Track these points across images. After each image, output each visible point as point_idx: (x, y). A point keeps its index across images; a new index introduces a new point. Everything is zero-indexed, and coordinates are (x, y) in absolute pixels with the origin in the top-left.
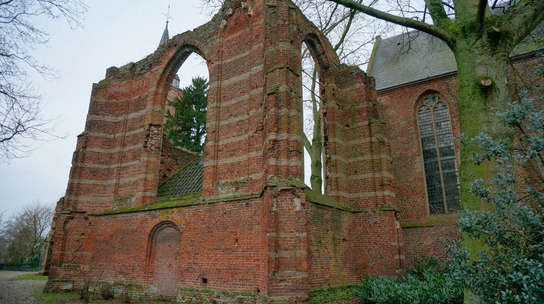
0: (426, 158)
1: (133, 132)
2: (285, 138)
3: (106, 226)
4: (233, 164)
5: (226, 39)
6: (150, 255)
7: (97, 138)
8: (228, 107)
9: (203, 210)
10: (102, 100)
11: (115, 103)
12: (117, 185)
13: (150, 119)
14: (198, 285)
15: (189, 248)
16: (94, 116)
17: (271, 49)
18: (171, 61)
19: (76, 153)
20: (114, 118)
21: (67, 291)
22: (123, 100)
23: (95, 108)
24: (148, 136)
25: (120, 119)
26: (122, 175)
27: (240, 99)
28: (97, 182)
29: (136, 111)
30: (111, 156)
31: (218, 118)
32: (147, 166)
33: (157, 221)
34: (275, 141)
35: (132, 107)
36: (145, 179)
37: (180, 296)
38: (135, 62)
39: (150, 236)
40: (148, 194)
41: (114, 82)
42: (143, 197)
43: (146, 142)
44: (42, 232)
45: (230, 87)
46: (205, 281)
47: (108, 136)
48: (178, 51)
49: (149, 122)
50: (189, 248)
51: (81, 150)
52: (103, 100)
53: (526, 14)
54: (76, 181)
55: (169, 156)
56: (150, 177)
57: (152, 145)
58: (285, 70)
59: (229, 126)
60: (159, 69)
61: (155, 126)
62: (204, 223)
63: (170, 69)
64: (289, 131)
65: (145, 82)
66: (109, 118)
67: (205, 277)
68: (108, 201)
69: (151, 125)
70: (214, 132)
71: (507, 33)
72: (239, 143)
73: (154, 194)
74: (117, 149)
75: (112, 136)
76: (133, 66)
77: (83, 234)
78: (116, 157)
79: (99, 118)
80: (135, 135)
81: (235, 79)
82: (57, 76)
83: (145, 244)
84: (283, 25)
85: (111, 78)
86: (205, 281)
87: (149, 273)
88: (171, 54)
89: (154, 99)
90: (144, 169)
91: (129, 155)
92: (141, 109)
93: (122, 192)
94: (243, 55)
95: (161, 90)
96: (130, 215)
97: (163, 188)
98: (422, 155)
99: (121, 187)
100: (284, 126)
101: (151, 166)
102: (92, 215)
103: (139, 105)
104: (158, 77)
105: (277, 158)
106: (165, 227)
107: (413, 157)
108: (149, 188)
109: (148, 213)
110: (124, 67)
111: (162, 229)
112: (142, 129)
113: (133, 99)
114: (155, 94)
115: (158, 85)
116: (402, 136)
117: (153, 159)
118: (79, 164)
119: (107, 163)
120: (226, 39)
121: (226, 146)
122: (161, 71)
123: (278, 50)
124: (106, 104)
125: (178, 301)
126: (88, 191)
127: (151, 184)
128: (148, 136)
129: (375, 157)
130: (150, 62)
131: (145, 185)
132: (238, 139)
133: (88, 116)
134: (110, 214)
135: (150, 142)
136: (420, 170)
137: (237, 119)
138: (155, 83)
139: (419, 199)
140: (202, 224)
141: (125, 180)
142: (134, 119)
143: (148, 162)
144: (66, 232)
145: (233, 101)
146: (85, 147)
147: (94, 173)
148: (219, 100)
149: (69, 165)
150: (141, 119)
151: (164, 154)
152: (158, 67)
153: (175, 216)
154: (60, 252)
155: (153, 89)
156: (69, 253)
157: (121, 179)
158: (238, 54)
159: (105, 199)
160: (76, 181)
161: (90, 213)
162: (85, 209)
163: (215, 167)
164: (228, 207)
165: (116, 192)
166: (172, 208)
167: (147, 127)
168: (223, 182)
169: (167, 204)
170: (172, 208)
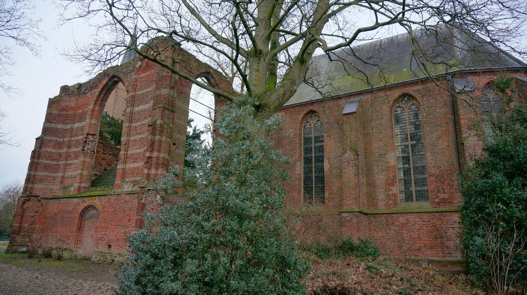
0: (305, 163)
1: (76, 138)
2: (156, 156)
3: (53, 207)
4: (134, 168)
5: (140, 76)
6: (80, 228)
7: (50, 141)
8: (135, 127)
10: (55, 112)
11: (66, 114)
12: (63, 177)
13: (87, 130)
14: (105, 250)
15: (103, 224)
17: (158, 92)
18: (104, 86)
19: (34, 152)
20: (64, 126)
21: (24, 252)
22: (71, 112)
23: (49, 118)
24: (85, 142)
25: (68, 127)
26: (67, 170)
27: (143, 122)
28: (49, 174)
29: (80, 122)
32: (83, 165)
33: (86, 205)
34: (149, 157)
35: (77, 118)
36: (81, 174)
37: (94, 257)
38: (82, 83)
39: (80, 215)
40: (83, 185)
41: (65, 98)
42: (79, 187)
43: (84, 147)
45: (138, 113)
46: (110, 246)
47: (59, 140)
48: (109, 80)
49: (87, 132)
50: (103, 224)
51: (38, 150)
52: (56, 112)
53: (279, 93)
54: (33, 173)
55: (110, 154)
56: (85, 172)
57: (88, 149)
58: (161, 109)
59: (135, 141)
60: (97, 91)
61: (91, 135)
62: (113, 208)
63: (104, 92)
64: (159, 151)
65: (87, 100)
66: (60, 126)
67: (110, 244)
68: (56, 189)
69: (88, 134)
70: (125, 144)
72: (140, 153)
74: (65, 150)
75: (62, 140)
76: (80, 85)
77: (36, 212)
78: (63, 156)
79: (52, 125)
80: (77, 141)
81: (142, 107)
82: (20, 93)
83: (77, 221)
84: (166, 76)
85: (63, 95)
86: (110, 246)
87: (79, 241)
88: (104, 82)
89: (92, 115)
90: (81, 167)
91: (73, 155)
92: (83, 121)
93: (66, 182)
94: (148, 90)
95: (97, 108)
96: (69, 199)
100: (156, 148)
101: (86, 165)
103: (82, 118)
104: (95, 99)
105: (150, 169)
106: (91, 210)
107: (295, 162)
108: (84, 180)
109: (80, 199)
110: (73, 86)
111: (89, 211)
112: (81, 137)
113: (78, 112)
114: (93, 111)
115: (95, 104)
116: (289, 145)
117: (88, 160)
118: (36, 161)
119: (57, 160)
120: (140, 76)
121: (132, 155)
122: (97, 93)
123: (161, 94)
125: (93, 259)
126: (41, 181)
127: (85, 178)
128: (85, 142)
130: (91, 85)
133: (44, 123)
134: (56, 198)
135: (87, 147)
136: (298, 172)
137: (140, 136)
138: (93, 103)
139: (296, 194)
140: (112, 208)
141: (68, 174)
142: (78, 128)
144: (24, 210)
145: (139, 123)
147: (47, 167)
148: (131, 122)
150: (82, 128)
151: (105, 152)
152: (95, 90)
153: (96, 202)
154: (18, 225)
155: (91, 107)
157: (66, 173)
158: (145, 88)
159: (54, 187)
160: (33, 173)
161: (42, 197)
162: (38, 194)
164: (128, 198)
165: (62, 182)
166: (95, 196)
167: (85, 136)
168: (127, 180)
169: (93, 193)
170: (95, 196)
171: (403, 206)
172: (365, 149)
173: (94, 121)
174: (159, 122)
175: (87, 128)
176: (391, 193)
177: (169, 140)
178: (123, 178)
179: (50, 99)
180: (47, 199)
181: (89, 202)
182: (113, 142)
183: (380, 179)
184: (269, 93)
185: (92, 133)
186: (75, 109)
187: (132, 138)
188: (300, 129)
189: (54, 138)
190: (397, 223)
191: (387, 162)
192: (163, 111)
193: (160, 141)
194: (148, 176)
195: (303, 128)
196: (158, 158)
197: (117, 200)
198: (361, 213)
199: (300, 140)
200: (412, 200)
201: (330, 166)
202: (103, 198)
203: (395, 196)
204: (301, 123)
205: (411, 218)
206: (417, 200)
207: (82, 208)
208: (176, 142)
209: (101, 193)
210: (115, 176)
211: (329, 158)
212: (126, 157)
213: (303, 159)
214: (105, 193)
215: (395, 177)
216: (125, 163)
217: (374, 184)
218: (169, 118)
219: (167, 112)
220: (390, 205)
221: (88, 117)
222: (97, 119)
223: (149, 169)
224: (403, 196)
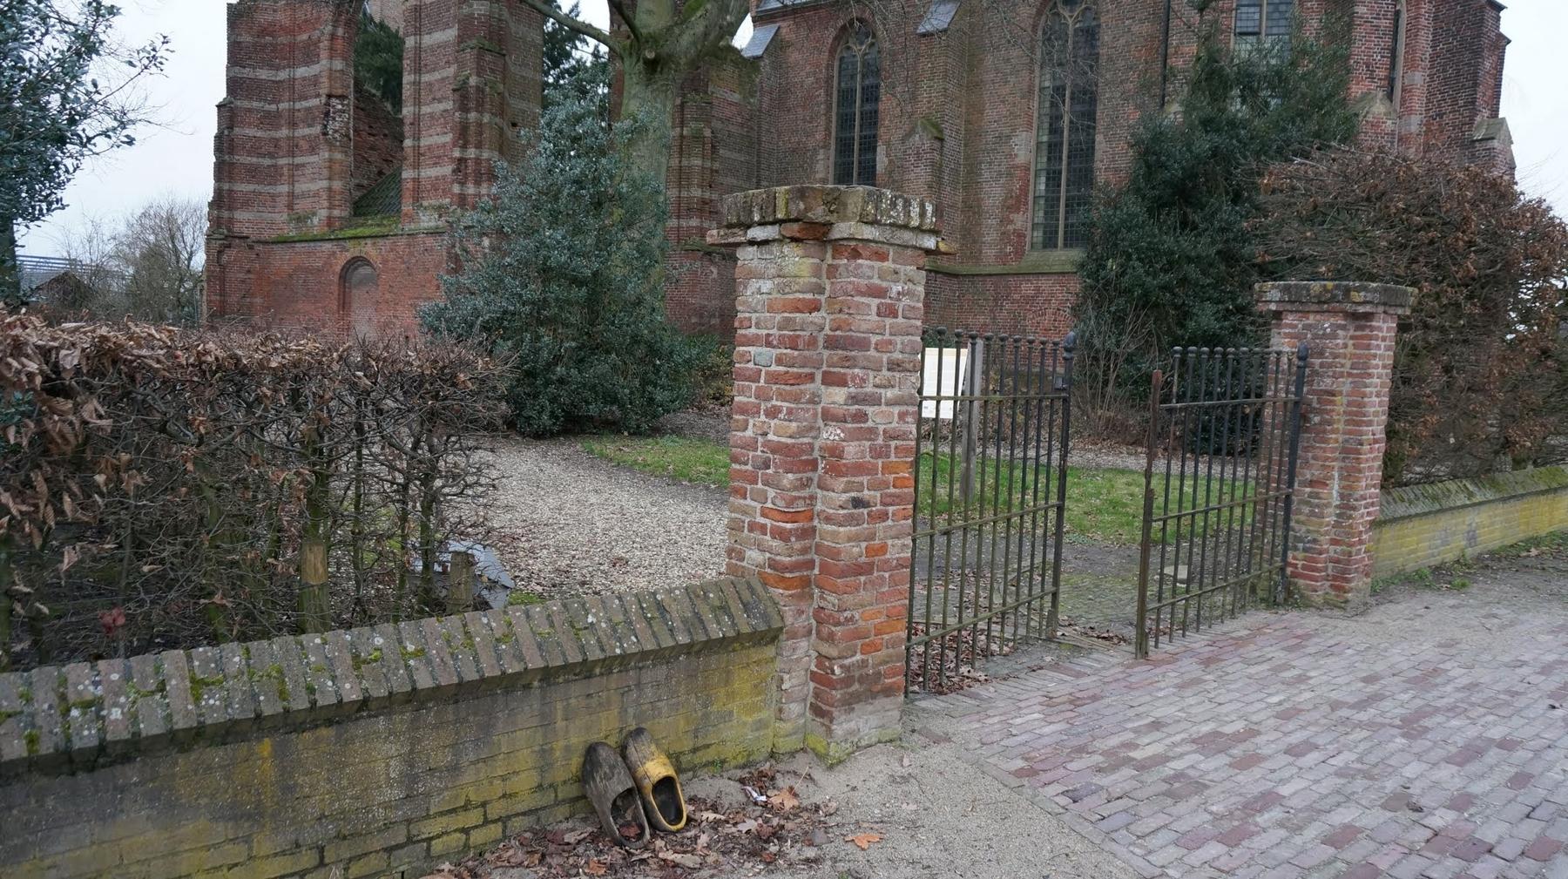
1: (305, 104)
3: (282, 260)
4: (437, 178)
6: (344, 304)
7: (249, 110)
8: (430, 84)
9: (403, 241)
12: (291, 195)
15: (388, 296)
16: (237, 69)
19: (218, 138)
23: (237, 54)
24: (327, 114)
25: (283, 75)
29: (307, 64)
30: (276, 142)
31: (418, 102)
33: (349, 255)
36: (330, 189)
40: (336, 213)
42: (329, 218)
44: (190, 259)
47: (267, 107)
50: (388, 296)
52: (249, 39)
59: (432, 116)
61: (337, 97)
64: (479, 146)
66: (264, 74)
68: (279, 221)
71: (670, 56)
74: (284, 132)
75: (274, 107)
79: (247, 72)
80: (308, 109)
83: (335, 288)
92: (314, 63)
93: (301, 206)
95: (340, 31)
98: (833, 147)
100: (472, 139)
101: (337, 167)
102: (259, 242)
103: (310, 57)
112: (316, 102)
116: (804, 107)
117: (338, 156)
119: (271, 156)
121: (429, 148)
123: (471, 16)
124: (254, 45)
126: (247, 204)
129: (685, 163)
131: (330, 198)
142: (304, 79)
146: (231, 128)
147: (253, 173)
149: (212, 159)
150: (315, 81)
153: (369, 249)
156: (233, 299)
160: (226, 187)
162: (246, 232)
163: (416, 180)
164: (430, 241)
168: (425, 203)
169: (359, 231)
171: (1033, 258)
172: (968, 122)
173: (338, 65)
174: (473, 81)
175: (324, 80)
176: (1010, 227)
177: (497, 120)
178: (417, 199)
179: (230, 6)
180: (266, 243)
181: (353, 250)
182: (389, 107)
183: (993, 194)
184: (677, 31)
185: (340, 92)
186: (290, 31)
187: (425, 109)
188: (829, 66)
189: (255, 104)
190: (1016, 296)
191: (1011, 156)
192: (479, 58)
193: (480, 125)
194: (462, 200)
195: (836, 64)
196: (478, 161)
197: (409, 245)
198: (937, 272)
199: (829, 94)
200: (1056, 246)
201: (890, 161)
202: (380, 242)
203: (1021, 236)
204: (832, 52)
205: (1045, 284)
206: (1065, 245)
207: (342, 262)
208: (519, 120)
209: (376, 230)
210: (399, 195)
211: (888, 144)
212: (418, 153)
213: (833, 141)
214: (385, 230)
215: (1024, 191)
216: (417, 166)
217: (979, 206)
218: (493, 71)
219: (488, 57)
220: (1007, 255)
221: (324, 54)
222: (345, 59)
223: (462, 184)
224: (1039, 234)
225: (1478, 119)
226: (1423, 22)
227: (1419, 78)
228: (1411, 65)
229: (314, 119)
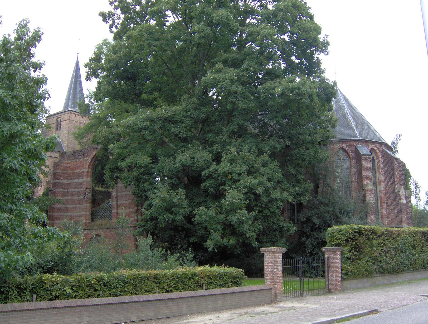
1: (77, 190)
7: (59, 192)
24: (85, 193)
29: (78, 179)
36: (86, 215)
40: (87, 221)
42: (86, 223)
47: (64, 191)
59: (122, 196)
66: (64, 181)
69: (86, 188)
73: (90, 221)
75: (66, 190)
89: (87, 175)
91: (76, 202)
92: (80, 178)
97: (93, 217)
99: (73, 216)
104: (88, 164)
112: (82, 189)
115: (89, 167)
122: (90, 161)
132: (126, 202)
138: (87, 167)
142: (77, 183)
143: (86, 206)
150: (81, 184)
189: (61, 190)
221: (85, 177)
225: (396, 186)
226: (381, 162)
227: (382, 176)
228: (379, 173)
229: (80, 194)
